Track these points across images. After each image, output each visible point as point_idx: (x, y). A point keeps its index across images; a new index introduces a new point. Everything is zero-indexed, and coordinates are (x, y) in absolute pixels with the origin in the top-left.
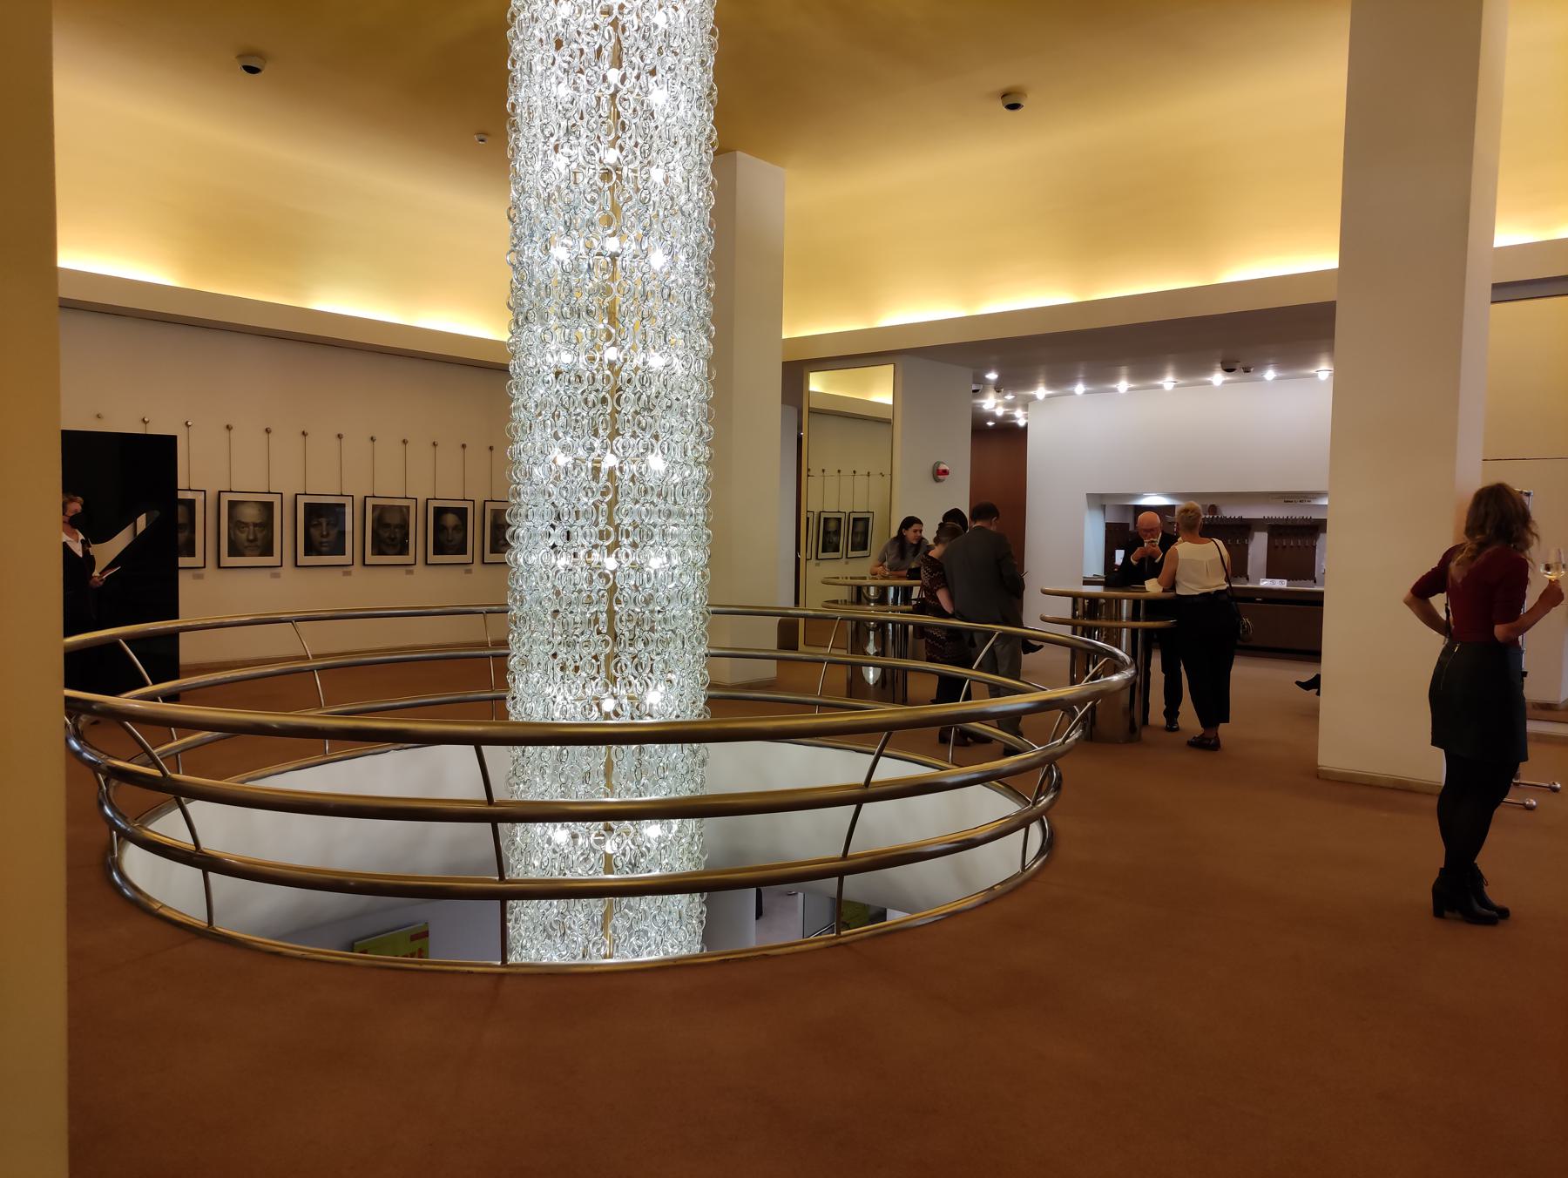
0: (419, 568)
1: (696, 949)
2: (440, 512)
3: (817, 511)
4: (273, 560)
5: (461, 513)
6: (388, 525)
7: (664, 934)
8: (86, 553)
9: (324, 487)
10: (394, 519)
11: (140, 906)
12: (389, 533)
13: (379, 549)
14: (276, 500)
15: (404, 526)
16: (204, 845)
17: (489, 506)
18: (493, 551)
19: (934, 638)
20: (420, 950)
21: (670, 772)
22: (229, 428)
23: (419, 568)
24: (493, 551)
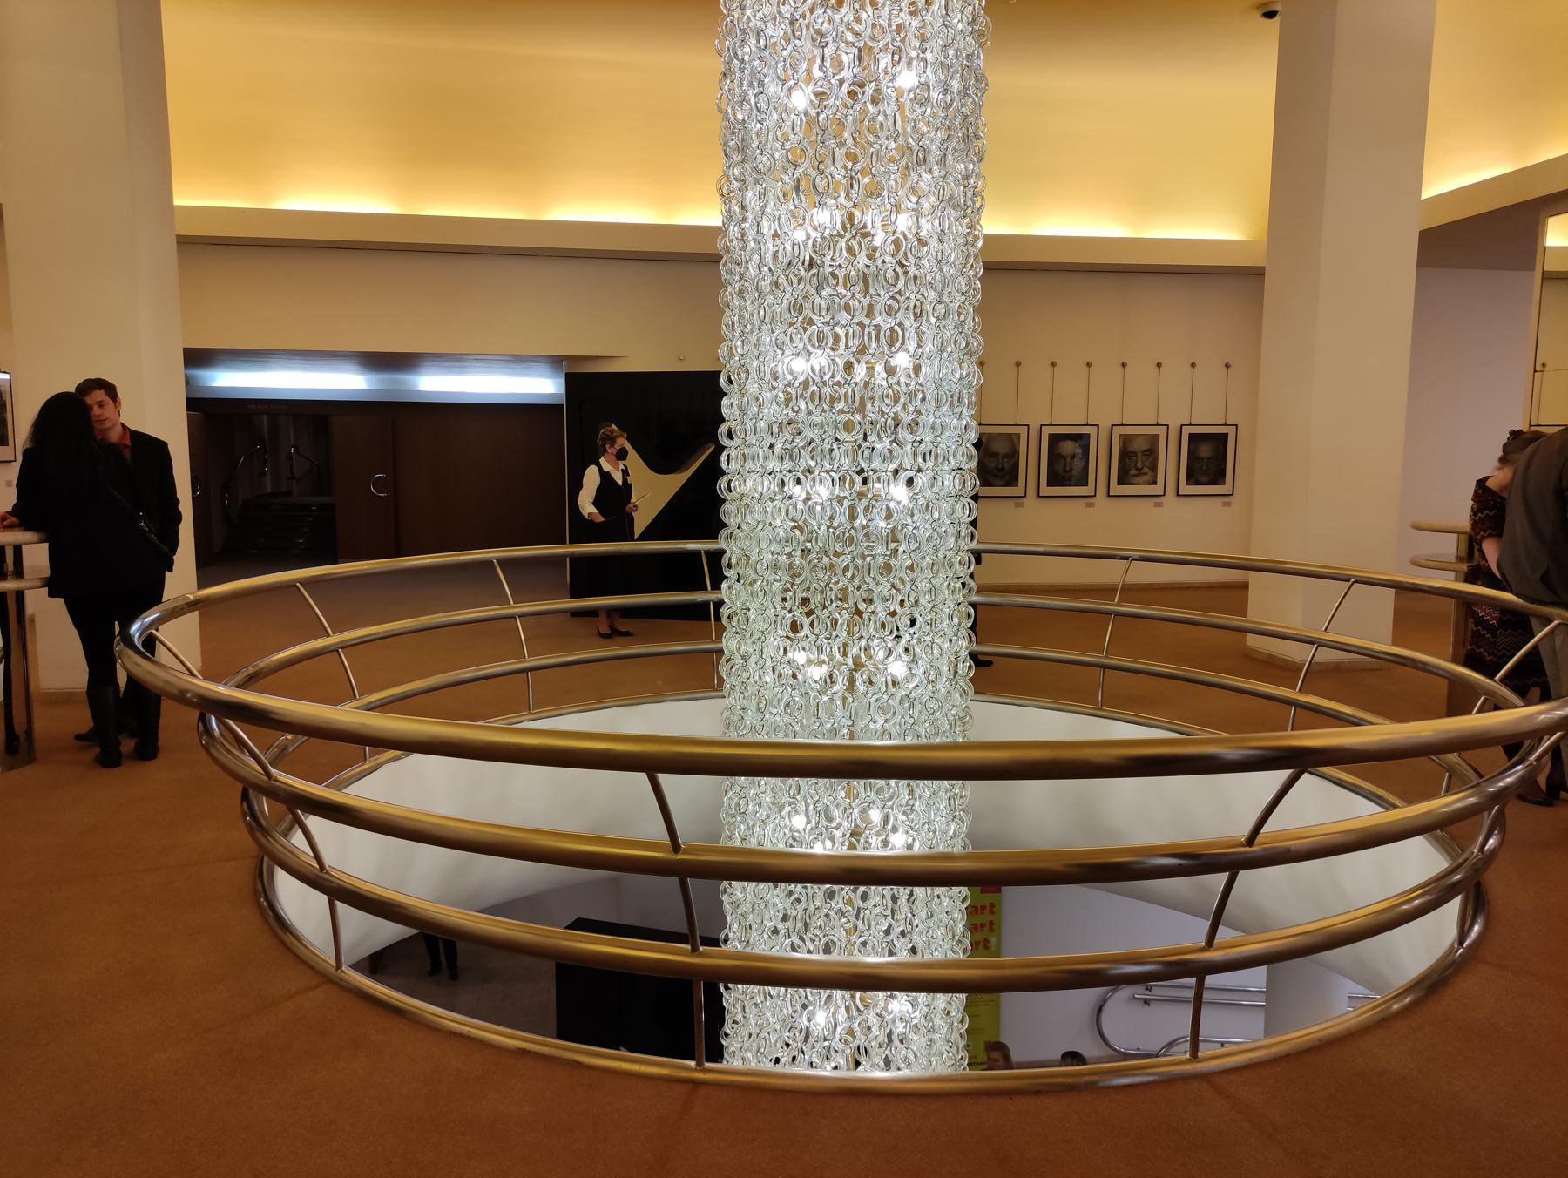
0: (1031, 500)
1: (963, 1069)
2: (1055, 440)
3: (1174, 426)
4: (1017, 491)
5: (1081, 439)
6: (995, 455)
7: (916, 1040)
8: (625, 481)
9: (1069, 417)
10: (1000, 448)
11: (279, 924)
12: (1136, 461)
13: (1193, 478)
14: (1022, 431)
15: (1014, 454)
16: (328, 861)
17: (1117, 432)
18: (1121, 482)
19: (1480, 622)
20: (992, 905)
21: (910, 822)
22: (1018, 364)
23: (1031, 500)
24: (1121, 482)
